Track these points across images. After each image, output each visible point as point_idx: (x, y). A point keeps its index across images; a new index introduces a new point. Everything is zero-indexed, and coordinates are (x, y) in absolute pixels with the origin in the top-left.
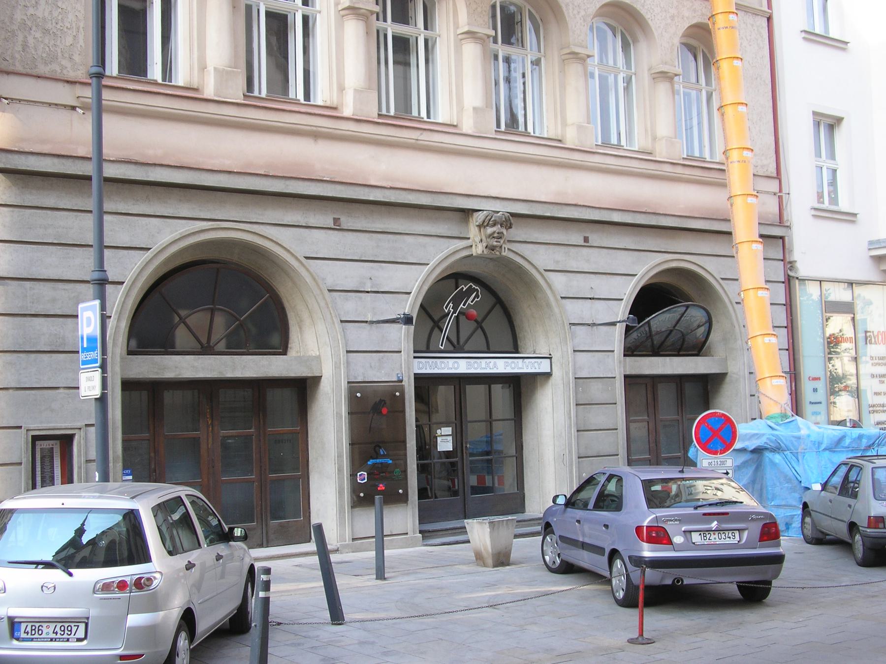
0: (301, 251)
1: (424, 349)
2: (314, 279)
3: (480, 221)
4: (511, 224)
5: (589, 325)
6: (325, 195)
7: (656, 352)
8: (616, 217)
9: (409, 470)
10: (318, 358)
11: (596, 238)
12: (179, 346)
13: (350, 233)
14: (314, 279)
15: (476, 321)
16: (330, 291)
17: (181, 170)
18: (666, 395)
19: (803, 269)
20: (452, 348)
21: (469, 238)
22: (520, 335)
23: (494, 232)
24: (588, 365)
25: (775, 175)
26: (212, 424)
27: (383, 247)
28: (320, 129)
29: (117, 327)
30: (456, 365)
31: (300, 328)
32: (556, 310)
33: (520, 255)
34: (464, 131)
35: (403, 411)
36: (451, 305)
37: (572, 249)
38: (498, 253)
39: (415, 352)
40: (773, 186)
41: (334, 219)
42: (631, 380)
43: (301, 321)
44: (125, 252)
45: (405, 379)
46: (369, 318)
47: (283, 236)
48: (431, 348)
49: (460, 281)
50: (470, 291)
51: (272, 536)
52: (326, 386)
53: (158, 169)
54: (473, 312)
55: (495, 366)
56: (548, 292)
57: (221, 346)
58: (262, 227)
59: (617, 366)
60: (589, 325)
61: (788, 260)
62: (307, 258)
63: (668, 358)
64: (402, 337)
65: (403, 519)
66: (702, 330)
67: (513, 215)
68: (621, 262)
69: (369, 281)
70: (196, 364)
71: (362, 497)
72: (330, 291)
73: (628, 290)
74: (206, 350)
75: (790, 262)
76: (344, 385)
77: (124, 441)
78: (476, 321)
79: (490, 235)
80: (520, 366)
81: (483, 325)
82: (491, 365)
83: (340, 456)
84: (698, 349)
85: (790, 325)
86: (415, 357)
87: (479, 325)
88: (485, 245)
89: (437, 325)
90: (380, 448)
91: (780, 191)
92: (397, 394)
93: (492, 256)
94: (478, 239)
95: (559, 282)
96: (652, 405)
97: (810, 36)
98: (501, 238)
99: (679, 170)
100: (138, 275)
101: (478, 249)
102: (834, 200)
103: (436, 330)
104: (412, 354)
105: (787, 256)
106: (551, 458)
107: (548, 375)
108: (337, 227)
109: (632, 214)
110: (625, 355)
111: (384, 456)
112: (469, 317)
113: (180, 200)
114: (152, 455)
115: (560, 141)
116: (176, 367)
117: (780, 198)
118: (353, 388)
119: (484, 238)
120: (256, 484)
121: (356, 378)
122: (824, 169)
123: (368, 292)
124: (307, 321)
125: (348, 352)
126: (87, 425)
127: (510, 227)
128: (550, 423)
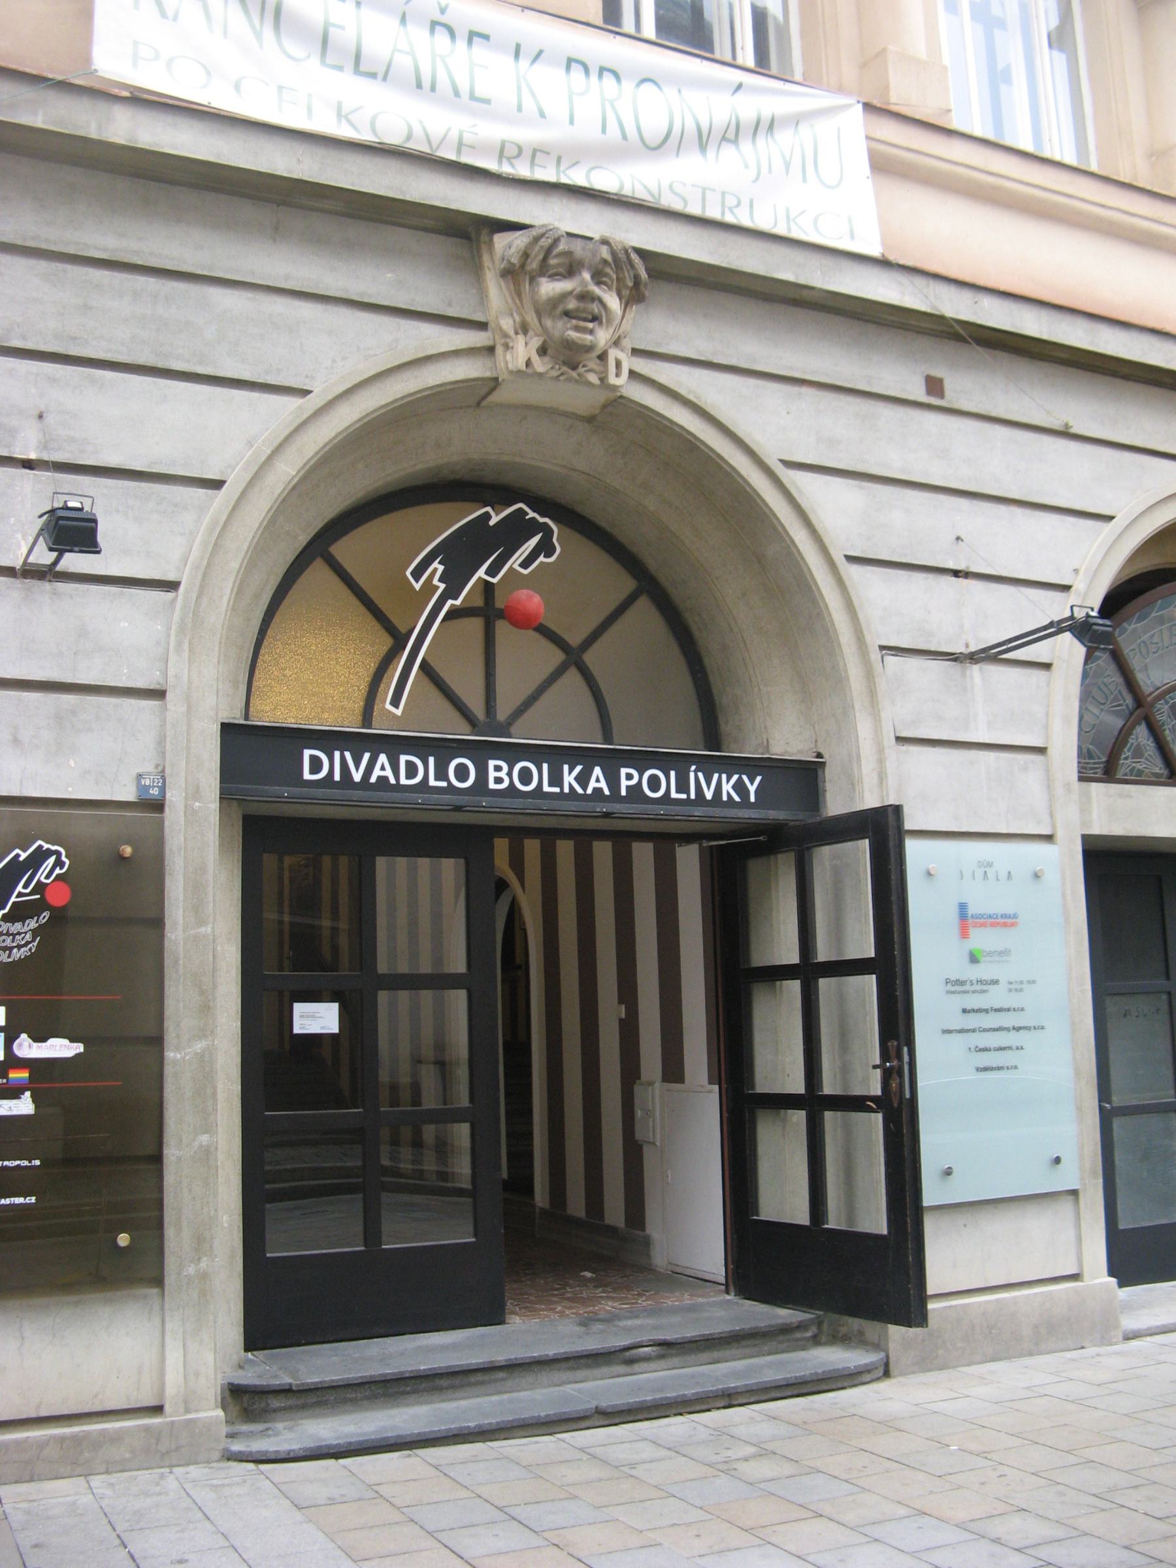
5: (954, 657)
11: (970, 385)
23: (564, 296)
27: (117, 315)
36: (438, 567)
45: (174, 798)
56: (800, 536)
87: (574, 657)
88: (536, 342)
94: (507, 324)
109: (1045, 315)
119: (532, 318)
123: (28, 464)
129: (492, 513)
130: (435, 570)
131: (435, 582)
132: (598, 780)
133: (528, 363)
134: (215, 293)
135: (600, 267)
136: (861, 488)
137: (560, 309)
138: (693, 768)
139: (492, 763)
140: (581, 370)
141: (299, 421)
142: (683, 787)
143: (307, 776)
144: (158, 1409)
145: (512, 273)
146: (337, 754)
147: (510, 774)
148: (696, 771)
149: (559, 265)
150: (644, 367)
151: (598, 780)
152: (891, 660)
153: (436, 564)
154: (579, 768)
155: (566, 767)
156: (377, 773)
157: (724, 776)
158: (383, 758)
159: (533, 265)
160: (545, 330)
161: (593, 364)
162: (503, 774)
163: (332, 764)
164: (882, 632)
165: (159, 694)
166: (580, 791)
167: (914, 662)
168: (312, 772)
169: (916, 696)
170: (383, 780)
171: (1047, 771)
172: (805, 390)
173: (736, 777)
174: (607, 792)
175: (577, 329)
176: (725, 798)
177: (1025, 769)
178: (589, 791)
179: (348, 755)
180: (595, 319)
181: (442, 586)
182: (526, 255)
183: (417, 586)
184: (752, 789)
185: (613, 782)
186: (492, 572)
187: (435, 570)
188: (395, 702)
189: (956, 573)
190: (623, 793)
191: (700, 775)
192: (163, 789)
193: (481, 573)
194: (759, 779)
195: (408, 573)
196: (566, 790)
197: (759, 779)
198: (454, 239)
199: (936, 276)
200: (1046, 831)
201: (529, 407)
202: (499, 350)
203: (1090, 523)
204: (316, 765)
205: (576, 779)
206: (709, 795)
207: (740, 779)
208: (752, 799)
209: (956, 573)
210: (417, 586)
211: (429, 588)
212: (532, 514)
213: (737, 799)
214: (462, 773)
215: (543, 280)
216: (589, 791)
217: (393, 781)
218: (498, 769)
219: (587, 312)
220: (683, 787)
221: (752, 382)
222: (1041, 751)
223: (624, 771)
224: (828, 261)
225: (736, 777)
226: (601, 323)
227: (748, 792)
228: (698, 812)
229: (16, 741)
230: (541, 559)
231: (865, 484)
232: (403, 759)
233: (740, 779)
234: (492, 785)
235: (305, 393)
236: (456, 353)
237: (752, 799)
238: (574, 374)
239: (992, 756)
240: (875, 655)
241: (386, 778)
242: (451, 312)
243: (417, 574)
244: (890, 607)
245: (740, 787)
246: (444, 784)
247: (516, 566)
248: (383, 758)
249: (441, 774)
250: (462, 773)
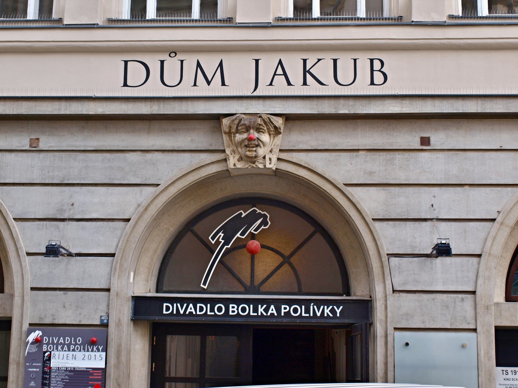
1: (296, 290)
11: (439, 137)
23: (243, 140)
33: (304, 167)
36: (221, 234)
38: (261, 166)
41: (422, 138)
47: (315, 161)
58: (295, 154)
62: (346, 185)
88: (237, 157)
95: (371, 201)
108: (34, 149)
109: (480, 101)
129: (243, 213)
130: (220, 236)
131: (220, 240)
132: (272, 310)
133: (235, 165)
135: (258, 126)
136: (384, 190)
137: (243, 144)
138: (312, 304)
139: (231, 306)
140: (257, 163)
141: (155, 196)
142: (307, 311)
143: (165, 312)
146: (175, 305)
147: (238, 309)
148: (313, 306)
149: (242, 129)
150: (284, 156)
151: (272, 310)
152: (393, 260)
153: (220, 234)
154: (265, 306)
155: (260, 306)
156: (189, 310)
157: (326, 307)
158: (191, 305)
159: (233, 130)
160: (239, 153)
162: (235, 309)
163: (173, 308)
164: (386, 249)
166: (265, 314)
168: (166, 311)
169: (405, 272)
170: (191, 313)
171: (475, 301)
173: (331, 307)
174: (276, 314)
175: (249, 151)
176: (326, 315)
178: (269, 314)
179: (179, 305)
180: (258, 146)
181: (223, 241)
182: (230, 127)
183: (213, 242)
184: (338, 311)
185: (278, 310)
187: (220, 236)
188: (204, 284)
190: (283, 314)
191: (315, 307)
192: (108, 320)
193: (238, 235)
194: (341, 307)
195: (210, 238)
196: (260, 314)
197: (341, 307)
198: (213, 121)
200: (472, 327)
201: (252, 174)
204: (168, 308)
205: (263, 310)
206: (319, 314)
207: (333, 308)
208: (338, 315)
210: (213, 242)
211: (218, 242)
212: (259, 211)
213: (331, 315)
214: (220, 309)
215: (237, 135)
216: (269, 314)
217: (194, 313)
218: (233, 307)
220: (307, 311)
221: (334, 154)
223: (283, 306)
224: (364, 102)
225: (331, 307)
226: (260, 147)
227: (337, 312)
228: (313, 321)
230: (263, 227)
231: (385, 188)
232: (198, 305)
233: (333, 308)
234: (231, 313)
235: (158, 185)
236: (213, 163)
237: (338, 315)
238: (254, 165)
240: (385, 258)
241: (192, 312)
243: (213, 238)
244: (391, 238)
245: (333, 311)
246: (213, 313)
247: (252, 231)
248: (191, 305)
249: (212, 310)
250: (220, 309)
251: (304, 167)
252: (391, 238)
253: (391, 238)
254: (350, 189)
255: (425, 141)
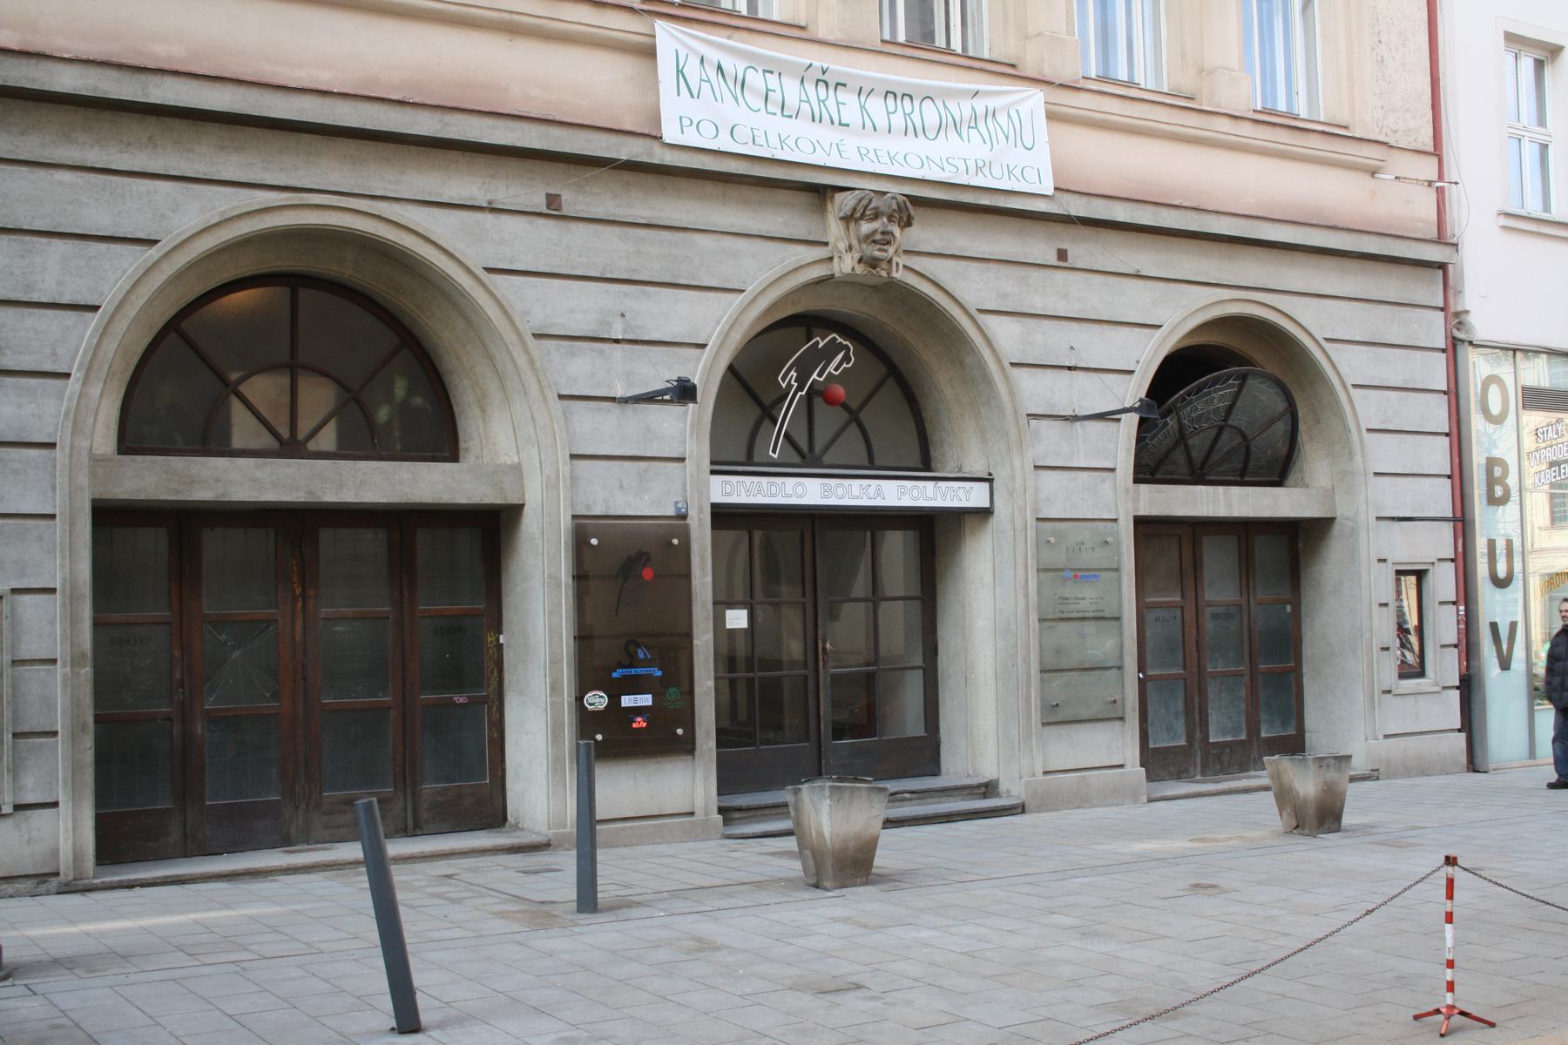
0: (477, 257)
1: (742, 458)
2: (506, 313)
3: (847, 209)
4: (910, 218)
5: (1065, 418)
6: (527, 145)
7: (1198, 475)
8: (1121, 213)
9: (697, 690)
10: (517, 469)
11: (1084, 250)
12: (237, 443)
13: (581, 225)
14: (506, 313)
15: (845, 406)
16: (538, 336)
17: (218, 85)
18: (1218, 559)
19: (1482, 325)
20: (797, 459)
21: (826, 244)
22: (934, 437)
23: (875, 232)
24: (1062, 496)
25: (1431, 149)
26: (304, 595)
27: (652, 256)
28: (515, 17)
29: (700, 520)
30: (800, 490)
31: (483, 411)
32: (1002, 388)
33: (929, 279)
34: (821, 35)
35: (687, 576)
36: (793, 373)
37: (1036, 274)
38: (884, 274)
39: (712, 463)
40: (1428, 169)
41: (548, 196)
42: (1147, 527)
43: (485, 396)
44: (102, 246)
45: (693, 513)
46: (620, 392)
48: (756, 459)
49: (815, 330)
50: (833, 349)
51: (424, 815)
52: (530, 524)
53: (170, 81)
54: (839, 390)
55: (879, 493)
56: (986, 353)
57: (327, 439)
59: (1122, 500)
60: (1065, 418)
61: (1452, 309)
63: (1221, 489)
64: (684, 430)
65: (688, 783)
66: (1281, 427)
67: (917, 201)
68: (1133, 300)
69: (619, 319)
70: (259, 475)
71: (608, 738)
72: (538, 336)
73: (1144, 356)
74: (291, 447)
75: (1457, 314)
76: (565, 522)
77: (97, 624)
78: (845, 406)
79: (868, 237)
80: (930, 494)
81: (861, 415)
82: (871, 491)
83: (555, 662)
84: (1278, 472)
85: (1455, 431)
86: (713, 472)
87: (854, 416)
88: (857, 256)
89: (768, 414)
90: (638, 645)
91: (1441, 178)
92: (675, 541)
93: (873, 281)
94: (842, 246)
95: (1007, 336)
96: (1191, 575)
97: (1517, 222)
98: (888, 243)
99: (1246, 129)
100: (129, 292)
101: (846, 265)
102: (1547, 208)
103: (767, 422)
104: (707, 466)
105: (1451, 300)
106: (990, 674)
107: (985, 514)
108: (553, 210)
109: (1152, 208)
110: (1136, 481)
111: (646, 663)
112: (830, 401)
113: (222, 148)
114: (177, 653)
115: (1013, 66)
116: (218, 481)
117: (1440, 191)
118: (582, 530)
119: (855, 243)
120: (392, 713)
121: (588, 507)
122: (1525, 142)
123: (617, 341)
124: (496, 397)
125: (573, 457)
126: (15, 591)
127: (909, 224)
128: (990, 603)
134: (698, 237)
144: (692, 814)
145: (848, 219)
152: (1033, 422)
159: (858, 215)
161: (884, 265)
165: (682, 460)
167: (1044, 423)
172: (991, 265)
177: (1103, 481)
186: (820, 375)
189: (1069, 368)
193: (815, 376)
199: (1068, 191)
202: (836, 260)
203: (1147, 331)
209: (1069, 368)
211: (790, 386)
219: (886, 239)
221: (963, 263)
222: (1113, 470)
229: (621, 487)
236: (815, 262)
239: (1085, 474)
242: (811, 238)
251: (929, 279)
252: (1036, 390)
253: (1036, 390)
254: (498, 278)
255: (552, 200)
